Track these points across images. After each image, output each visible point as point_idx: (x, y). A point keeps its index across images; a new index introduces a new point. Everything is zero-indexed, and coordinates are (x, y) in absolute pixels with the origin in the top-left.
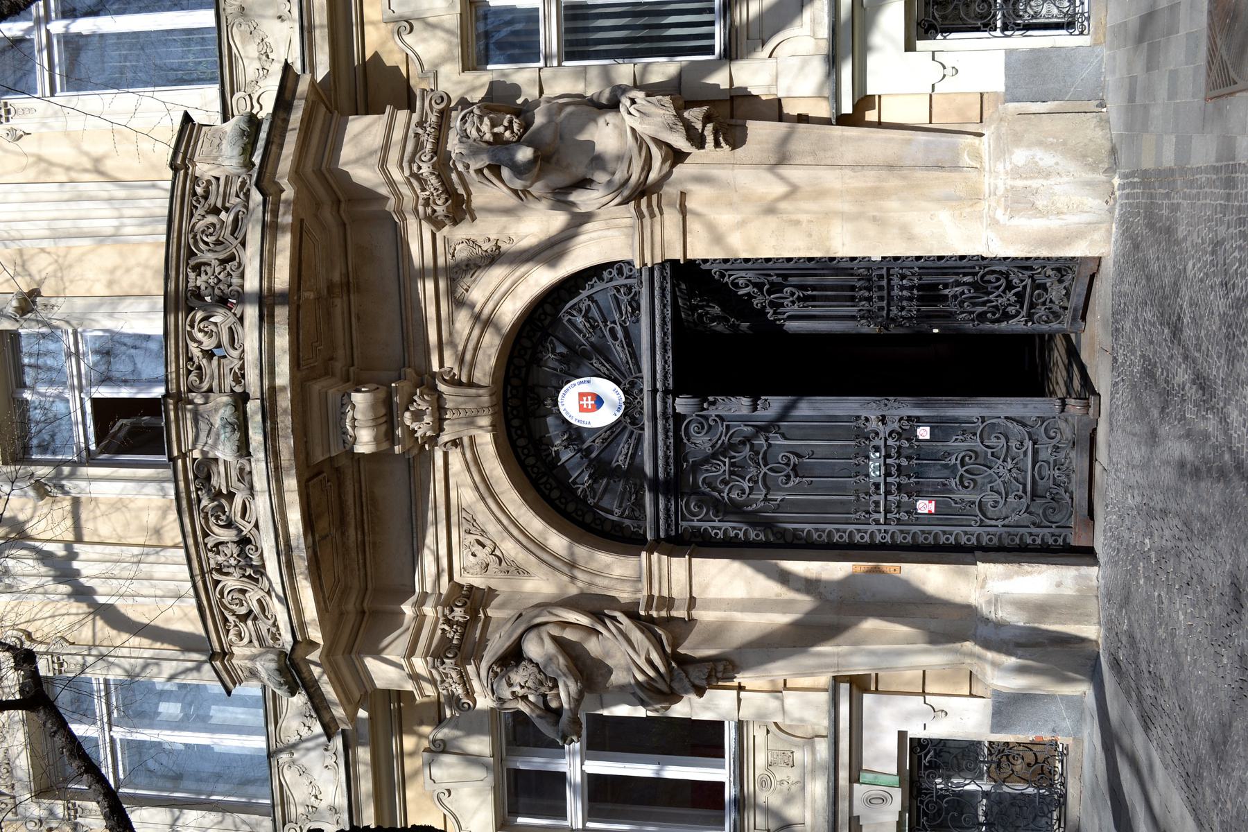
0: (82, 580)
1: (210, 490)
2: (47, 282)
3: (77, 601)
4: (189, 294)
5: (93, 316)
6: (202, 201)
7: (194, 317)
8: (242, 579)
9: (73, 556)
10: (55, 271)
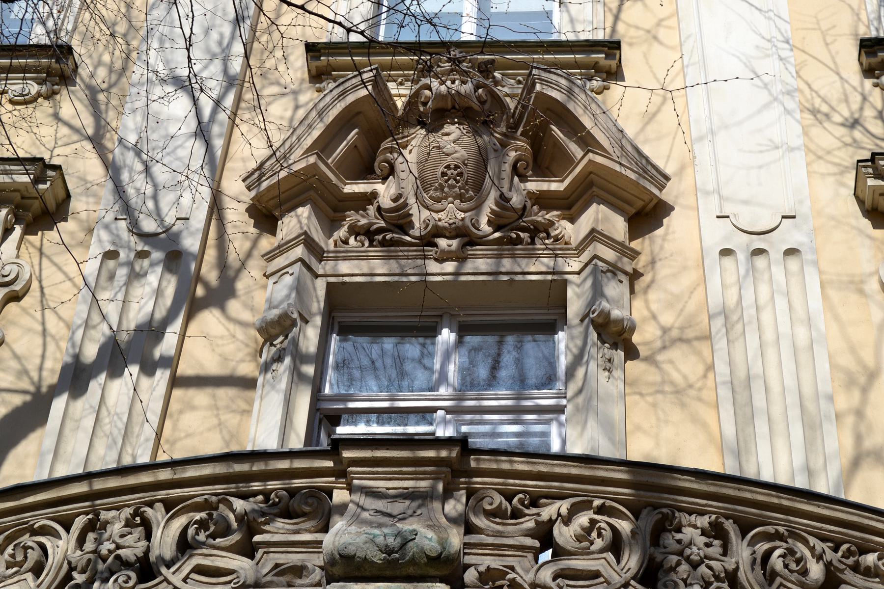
0: (103, 377)
1: (263, 514)
2: (653, 369)
3: (65, 368)
4: (665, 510)
5: (592, 423)
6: (851, 561)
7: (622, 516)
8: (66, 566)
9: (149, 368)
10: (672, 383)
